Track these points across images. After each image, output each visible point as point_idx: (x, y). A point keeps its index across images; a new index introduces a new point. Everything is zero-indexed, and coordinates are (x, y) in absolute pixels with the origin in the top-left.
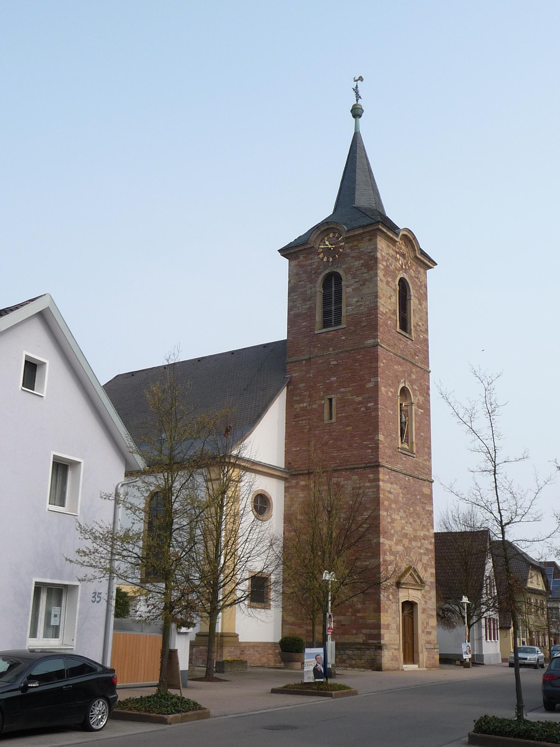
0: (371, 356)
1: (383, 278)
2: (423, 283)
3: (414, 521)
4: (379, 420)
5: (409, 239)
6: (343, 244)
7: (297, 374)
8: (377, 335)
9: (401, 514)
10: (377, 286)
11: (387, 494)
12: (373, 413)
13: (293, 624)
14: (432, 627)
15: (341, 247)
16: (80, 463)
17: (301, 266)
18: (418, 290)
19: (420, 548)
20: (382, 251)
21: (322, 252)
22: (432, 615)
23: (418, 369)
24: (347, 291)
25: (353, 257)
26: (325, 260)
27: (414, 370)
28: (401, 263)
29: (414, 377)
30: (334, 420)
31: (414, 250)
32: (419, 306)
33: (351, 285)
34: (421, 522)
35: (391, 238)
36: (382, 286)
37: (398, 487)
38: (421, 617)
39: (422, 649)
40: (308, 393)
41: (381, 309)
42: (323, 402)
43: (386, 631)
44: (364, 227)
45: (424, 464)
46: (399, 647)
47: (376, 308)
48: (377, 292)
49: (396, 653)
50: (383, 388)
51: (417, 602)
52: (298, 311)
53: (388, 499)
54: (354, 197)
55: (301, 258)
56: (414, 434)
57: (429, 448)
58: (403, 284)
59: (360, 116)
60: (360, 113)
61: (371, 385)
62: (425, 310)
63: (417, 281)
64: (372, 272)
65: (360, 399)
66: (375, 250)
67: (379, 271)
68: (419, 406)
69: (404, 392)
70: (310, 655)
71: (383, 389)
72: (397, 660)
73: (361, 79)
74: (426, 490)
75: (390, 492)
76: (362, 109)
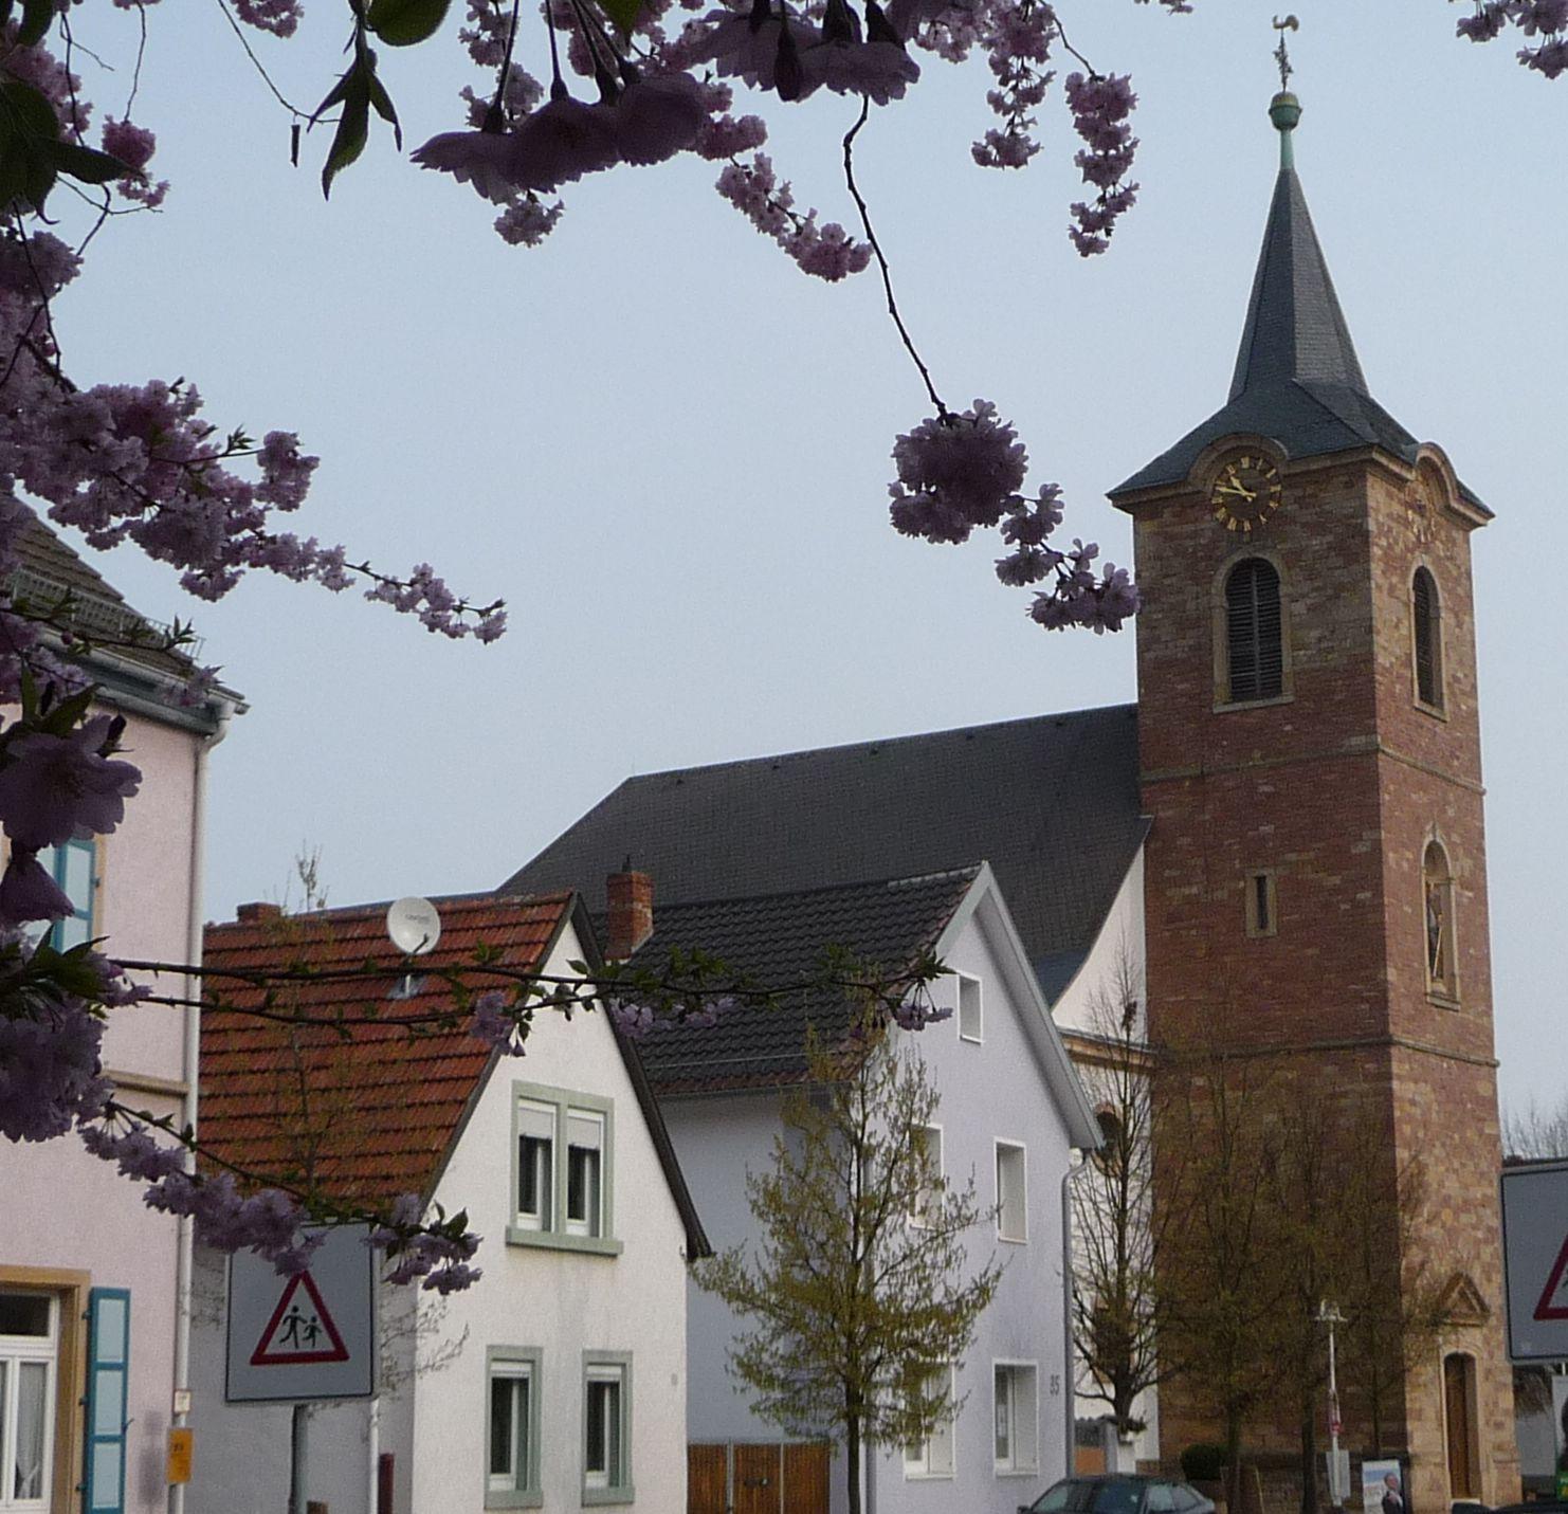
0: (1362, 776)
1: (1381, 581)
2: (1463, 570)
3: (1463, 1165)
4: (1387, 933)
5: (1435, 468)
6: (1279, 488)
7: (1170, 813)
8: (1375, 726)
9: (1436, 1151)
10: (1369, 602)
11: (1407, 1107)
12: (1369, 916)
13: (1189, 1415)
14: (1506, 1412)
15: (1272, 496)
16: (1020, 1150)
17: (1169, 538)
18: (1454, 589)
19: (1475, 1228)
20: (1377, 511)
21: (1223, 505)
22: (1505, 1385)
23: (1460, 791)
24: (1294, 608)
25: (1304, 525)
26: (1232, 525)
27: (1451, 797)
28: (1415, 530)
29: (1451, 812)
30: (1272, 930)
31: (1444, 491)
32: (1457, 630)
33: (1303, 596)
34: (1476, 1166)
35: (1396, 475)
36: (1379, 599)
37: (1429, 1088)
38: (1482, 1389)
39: (1488, 1462)
40: (1200, 862)
41: (1382, 660)
42: (1242, 884)
43: (1417, 1424)
44: (1334, 454)
45: (1477, 1025)
46: (1443, 1459)
47: (1369, 658)
48: (1371, 619)
49: (1437, 1472)
50: (1391, 855)
51: (1474, 1354)
52: (1168, 652)
53: (1410, 1119)
54: (1295, 357)
55: (1167, 514)
56: (1456, 954)
57: (1488, 983)
58: (1423, 580)
59: (1294, 125)
60: (1293, 120)
61: (1361, 848)
62: (1468, 638)
63: (1451, 567)
64: (1355, 567)
65: (1336, 880)
66: (1363, 511)
67: (1373, 566)
68: (1465, 885)
69: (1434, 852)
70: (1374, 1475)
71: (1391, 857)
72: (1440, 1488)
73: (1292, 22)
74: (1483, 1089)
75: (1413, 1103)
76: (1298, 108)
